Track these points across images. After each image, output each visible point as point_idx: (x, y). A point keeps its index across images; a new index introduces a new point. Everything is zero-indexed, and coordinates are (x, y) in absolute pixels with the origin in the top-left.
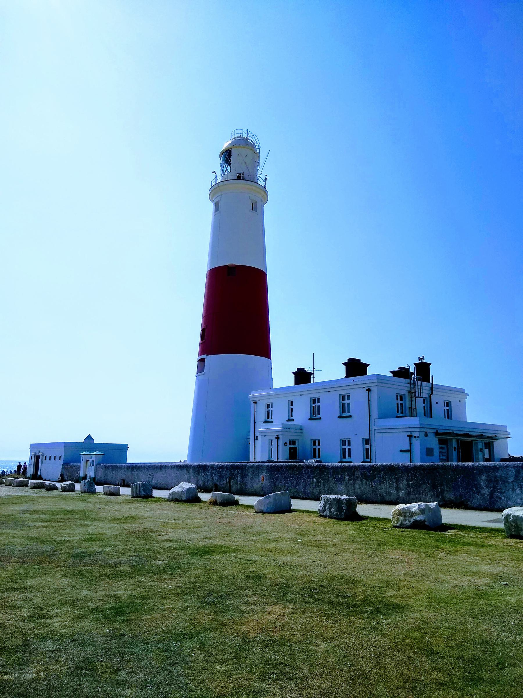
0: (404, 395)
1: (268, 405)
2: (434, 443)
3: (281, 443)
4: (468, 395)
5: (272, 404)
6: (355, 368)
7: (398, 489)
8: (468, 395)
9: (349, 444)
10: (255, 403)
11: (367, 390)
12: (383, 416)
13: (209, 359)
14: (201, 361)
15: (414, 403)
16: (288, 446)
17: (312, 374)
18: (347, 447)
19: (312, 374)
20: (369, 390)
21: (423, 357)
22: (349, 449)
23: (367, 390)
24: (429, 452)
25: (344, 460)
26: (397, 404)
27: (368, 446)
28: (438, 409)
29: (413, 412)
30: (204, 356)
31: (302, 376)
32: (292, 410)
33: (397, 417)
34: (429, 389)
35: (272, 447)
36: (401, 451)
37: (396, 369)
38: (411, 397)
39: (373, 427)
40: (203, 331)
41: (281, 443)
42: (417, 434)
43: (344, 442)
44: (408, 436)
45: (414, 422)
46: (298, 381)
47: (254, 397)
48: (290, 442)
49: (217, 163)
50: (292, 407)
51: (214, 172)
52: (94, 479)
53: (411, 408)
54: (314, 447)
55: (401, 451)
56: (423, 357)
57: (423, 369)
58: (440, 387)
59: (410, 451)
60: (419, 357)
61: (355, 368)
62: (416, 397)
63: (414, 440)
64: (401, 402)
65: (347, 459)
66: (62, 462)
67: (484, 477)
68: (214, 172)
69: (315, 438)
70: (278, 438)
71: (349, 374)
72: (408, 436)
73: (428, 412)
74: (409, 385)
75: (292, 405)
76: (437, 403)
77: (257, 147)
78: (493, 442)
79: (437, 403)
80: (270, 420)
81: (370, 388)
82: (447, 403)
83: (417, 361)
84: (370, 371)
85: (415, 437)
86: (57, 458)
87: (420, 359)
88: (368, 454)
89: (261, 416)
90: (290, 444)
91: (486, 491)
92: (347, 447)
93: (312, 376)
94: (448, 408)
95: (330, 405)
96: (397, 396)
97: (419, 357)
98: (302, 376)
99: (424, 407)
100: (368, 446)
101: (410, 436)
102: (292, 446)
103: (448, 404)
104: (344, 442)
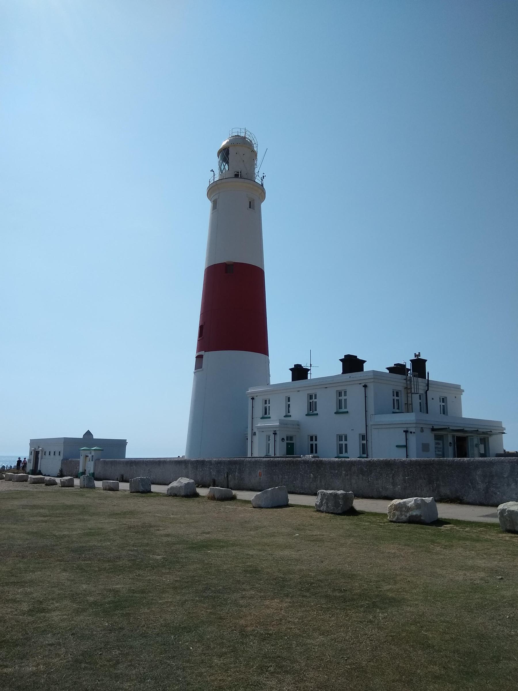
0: (400, 391)
1: (266, 401)
2: (429, 438)
3: (278, 438)
4: (463, 391)
5: (269, 400)
6: (352, 364)
7: (394, 484)
8: (463, 391)
9: (346, 440)
10: (253, 399)
11: (363, 386)
12: (379, 411)
13: (207, 355)
14: (199, 358)
15: (410, 399)
16: (286, 441)
17: (309, 370)
18: (343, 442)
19: (309, 370)
20: (365, 386)
21: (419, 353)
22: (346, 445)
23: (363, 386)
24: (425, 447)
25: (341, 455)
26: (394, 400)
27: (365, 442)
28: (434, 405)
29: (409, 408)
30: (202, 353)
31: (299, 373)
32: (289, 406)
33: (394, 413)
34: (425, 385)
35: (269, 442)
36: (397, 446)
37: (392, 365)
38: (407, 393)
39: (370, 423)
40: (201, 328)
41: (278, 438)
42: (413, 430)
43: (340, 438)
44: (404, 431)
45: (409, 418)
46: (295, 377)
47: (252, 393)
48: (287, 437)
49: (215, 162)
50: (289, 403)
51: (212, 171)
52: (93, 474)
53: (407, 404)
54: (312, 442)
55: (397, 446)
56: (419, 353)
57: (419, 365)
58: (436, 383)
59: (406, 446)
60: (415, 354)
61: (352, 364)
62: (412, 394)
63: (410, 436)
64: (397, 398)
65: (344, 455)
66: (61, 457)
67: (479, 472)
68: (212, 171)
69: (313, 433)
70: (275, 434)
71: (345, 370)
72: (404, 431)
73: (425, 408)
74: (405, 381)
75: (289, 401)
76: (433, 399)
77: (255, 146)
78: (488, 437)
79: (433, 399)
80: (267, 416)
81: (367, 384)
82: (443, 399)
83: (413, 358)
84: (366, 367)
85: (411, 432)
86: (57, 454)
87: (416, 355)
88: (364, 449)
89: (259, 412)
90: (287, 440)
91: (481, 486)
92: (343, 442)
93: (309, 372)
94: (443, 404)
95: (326, 403)
96: (393, 392)
97: (415, 354)
98: (299, 373)
99: (420, 403)
100: (365, 442)
101: (406, 432)
102: (289, 442)
103: (444, 400)
104: (340, 438)
